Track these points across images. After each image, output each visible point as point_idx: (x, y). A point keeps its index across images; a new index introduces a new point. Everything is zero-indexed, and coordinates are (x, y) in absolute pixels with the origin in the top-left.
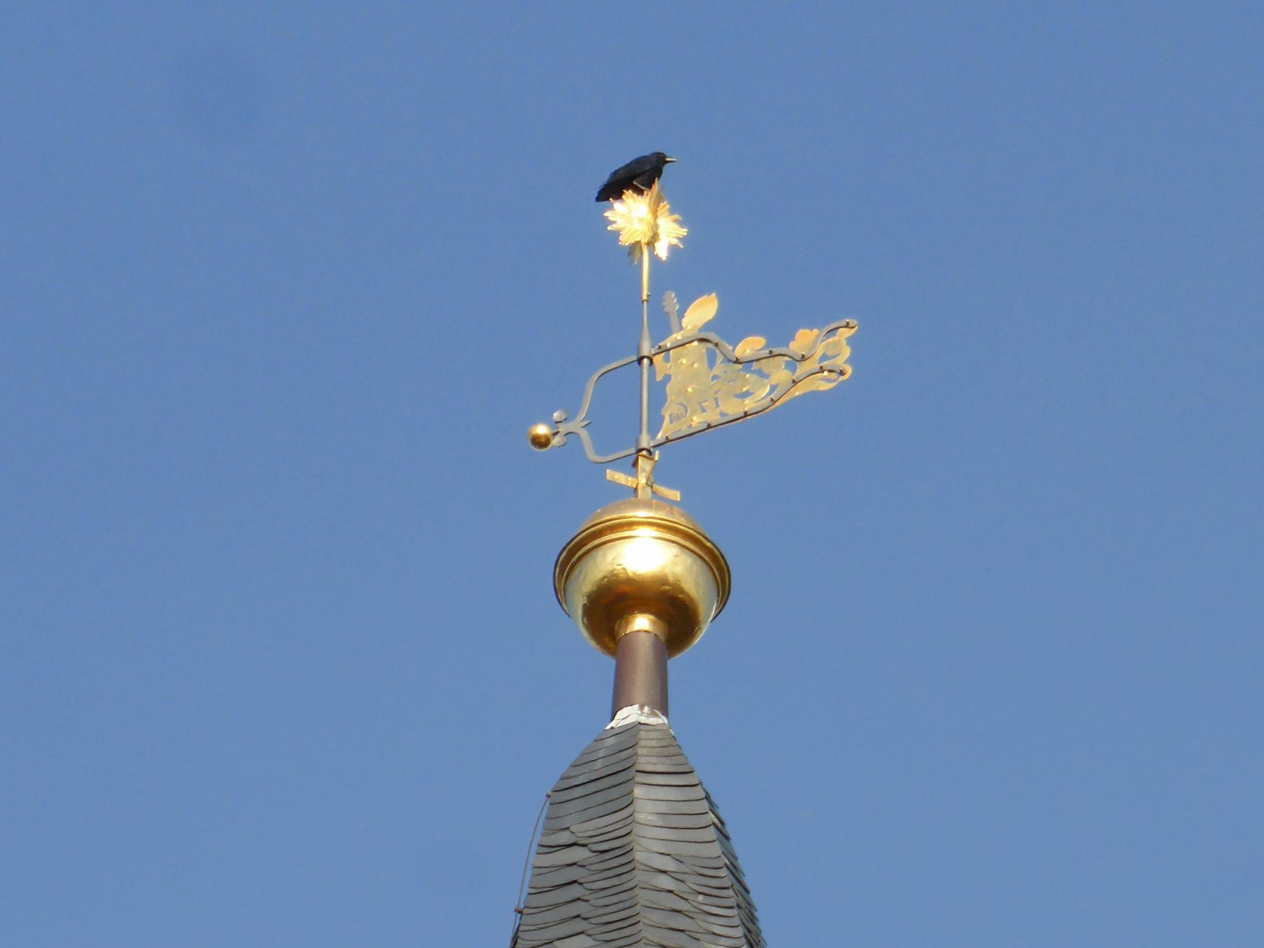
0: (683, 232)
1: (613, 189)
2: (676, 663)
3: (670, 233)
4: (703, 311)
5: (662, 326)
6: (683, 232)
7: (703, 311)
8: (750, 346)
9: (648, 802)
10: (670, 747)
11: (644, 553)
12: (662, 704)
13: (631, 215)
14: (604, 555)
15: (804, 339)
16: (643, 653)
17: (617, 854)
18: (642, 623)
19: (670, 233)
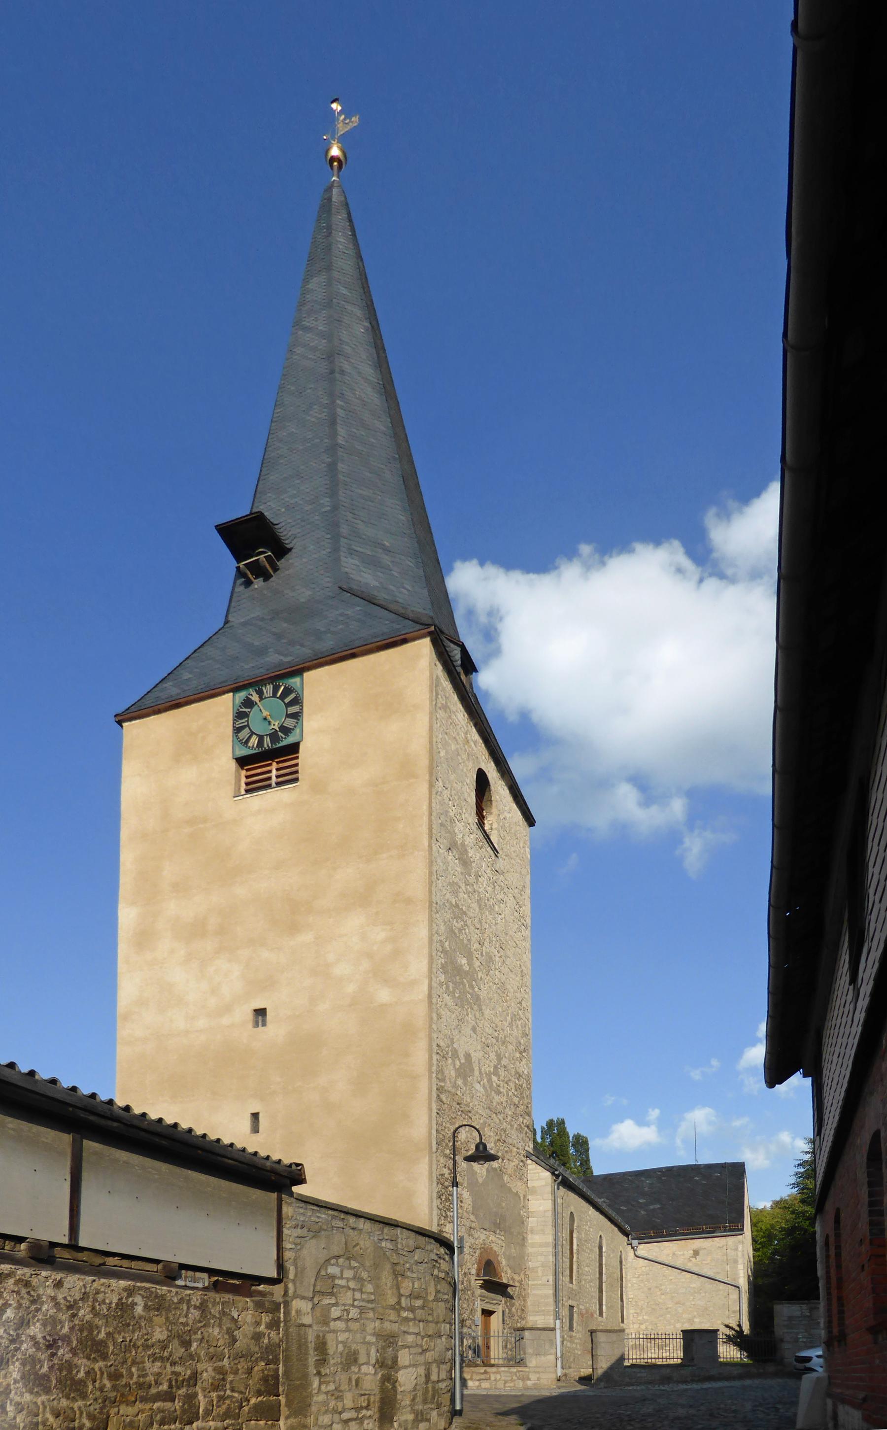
0: (650, 1110)
1: (332, 102)
2: (341, 173)
3: (339, 108)
4: (343, 117)
5: (338, 120)
6: (650, 1110)
7: (343, 117)
8: (347, 121)
9: (335, 191)
10: (338, 182)
11: (335, 151)
12: (338, 177)
13: (334, 106)
14: (479, 688)
15: (353, 119)
16: (335, 168)
17: (330, 199)
18: (335, 164)
19: (339, 108)
